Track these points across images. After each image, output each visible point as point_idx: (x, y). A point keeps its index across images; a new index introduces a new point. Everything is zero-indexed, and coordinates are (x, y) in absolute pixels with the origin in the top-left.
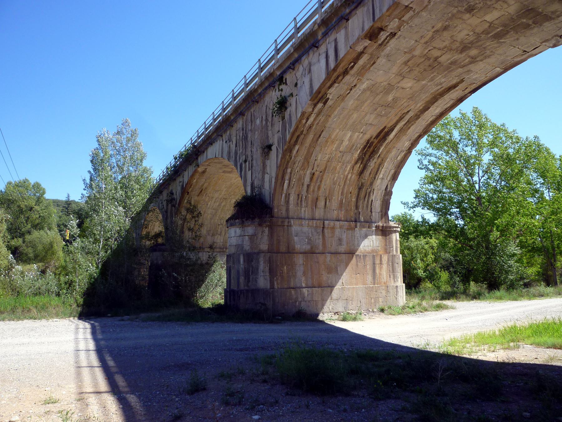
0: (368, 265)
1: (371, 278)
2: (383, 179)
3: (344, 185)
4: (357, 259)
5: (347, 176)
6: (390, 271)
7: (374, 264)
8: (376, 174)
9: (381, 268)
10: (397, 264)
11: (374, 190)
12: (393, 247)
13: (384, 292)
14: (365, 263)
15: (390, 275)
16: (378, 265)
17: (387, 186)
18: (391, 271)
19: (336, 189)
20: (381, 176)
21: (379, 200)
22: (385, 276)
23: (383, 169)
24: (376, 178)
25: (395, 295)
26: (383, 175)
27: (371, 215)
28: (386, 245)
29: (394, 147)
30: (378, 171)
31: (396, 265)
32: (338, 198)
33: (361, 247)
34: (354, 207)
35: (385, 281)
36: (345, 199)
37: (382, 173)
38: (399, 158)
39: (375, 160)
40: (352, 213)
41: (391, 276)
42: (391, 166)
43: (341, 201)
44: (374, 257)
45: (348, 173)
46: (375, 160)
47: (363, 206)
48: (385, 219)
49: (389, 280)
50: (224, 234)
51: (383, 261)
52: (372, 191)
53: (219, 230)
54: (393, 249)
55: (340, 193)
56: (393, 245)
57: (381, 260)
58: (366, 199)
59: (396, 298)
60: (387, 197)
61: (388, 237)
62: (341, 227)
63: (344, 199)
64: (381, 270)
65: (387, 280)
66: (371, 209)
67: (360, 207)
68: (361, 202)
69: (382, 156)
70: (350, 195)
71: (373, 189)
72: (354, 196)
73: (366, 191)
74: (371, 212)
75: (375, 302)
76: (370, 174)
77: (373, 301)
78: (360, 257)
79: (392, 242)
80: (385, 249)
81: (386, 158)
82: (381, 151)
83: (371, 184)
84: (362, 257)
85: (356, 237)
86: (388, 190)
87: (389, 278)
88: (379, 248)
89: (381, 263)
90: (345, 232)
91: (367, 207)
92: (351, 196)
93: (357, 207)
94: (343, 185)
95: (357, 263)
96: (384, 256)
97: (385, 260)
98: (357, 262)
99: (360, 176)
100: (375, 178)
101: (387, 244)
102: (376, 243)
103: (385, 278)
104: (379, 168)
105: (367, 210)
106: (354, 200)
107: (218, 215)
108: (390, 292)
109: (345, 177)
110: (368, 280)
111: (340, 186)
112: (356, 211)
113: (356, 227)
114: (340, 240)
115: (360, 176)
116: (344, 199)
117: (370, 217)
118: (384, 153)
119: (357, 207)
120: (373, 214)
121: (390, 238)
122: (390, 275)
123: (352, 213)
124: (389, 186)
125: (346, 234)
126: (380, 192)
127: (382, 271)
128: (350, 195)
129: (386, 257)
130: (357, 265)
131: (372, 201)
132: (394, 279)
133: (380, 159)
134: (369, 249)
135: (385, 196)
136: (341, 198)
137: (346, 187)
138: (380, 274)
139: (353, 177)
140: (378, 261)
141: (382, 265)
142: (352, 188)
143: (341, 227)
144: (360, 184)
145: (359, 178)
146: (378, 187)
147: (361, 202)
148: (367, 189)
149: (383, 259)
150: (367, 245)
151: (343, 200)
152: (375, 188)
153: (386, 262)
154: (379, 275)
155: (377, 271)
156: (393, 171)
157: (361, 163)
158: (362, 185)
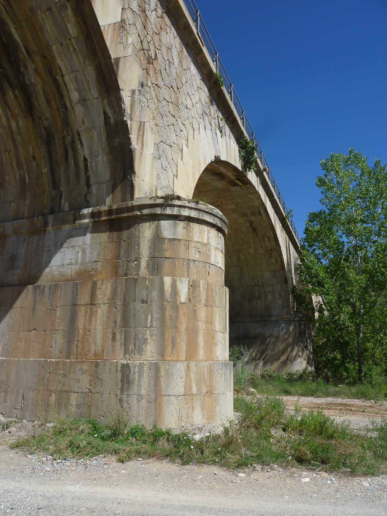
0: (58, 309)
1: (62, 341)
2: (83, 101)
3: (15, 146)
4: (35, 297)
5: (10, 127)
6: (115, 323)
7: (74, 305)
8: (61, 96)
9: (91, 316)
10: (143, 302)
11: (79, 135)
12: (138, 259)
13: (85, 380)
14: (53, 304)
15: (114, 334)
16: (83, 308)
17: (105, 113)
18: (118, 324)
19: (4, 160)
20: (75, 96)
21: (100, 152)
22: (99, 335)
23: (66, 78)
24: (69, 106)
25: (119, 392)
26: (78, 90)
27: (89, 191)
28: (118, 257)
29: (32, 10)
30: (58, 87)
31: (138, 305)
32: (15, 176)
33: (56, 260)
34: (49, 186)
35: (99, 348)
36: (28, 174)
37: (71, 86)
38: (72, 30)
39: (29, 67)
40: (46, 199)
41: (118, 337)
42: (76, 62)
43: (23, 179)
44: (77, 289)
45: (8, 120)
46: (30, 66)
47: (69, 178)
48: (124, 194)
49: (110, 349)
50: (264, 297)
51: (99, 297)
52: (76, 137)
53: (256, 293)
54: (138, 266)
55: (14, 164)
56: (139, 253)
57: (93, 295)
58: (71, 161)
59: (121, 400)
60: (117, 141)
61: (125, 233)
62: (16, 232)
63: (26, 175)
64: (90, 320)
65: (103, 346)
66: (88, 178)
67: (63, 181)
68: (62, 170)
69: (33, 47)
70: (34, 164)
71: (75, 132)
72: (43, 162)
73: (64, 142)
74: (88, 185)
75: (59, 403)
76: (48, 102)
77: (53, 399)
78: (44, 290)
79: (139, 245)
80: (115, 267)
81: (48, 47)
82: (16, 36)
83: (66, 122)
84: (47, 290)
85: (46, 248)
86: (112, 120)
87: (110, 341)
88: (99, 265)
89: (92, 304)
90: (24, 241)
91: (78, 176)
92: (37, 165)
93: (55, 184)
94: (12, 148)
95: (34, 305)
96: (102, 284)
97: (105, 295)
98: (35, 301)
99: (32, 115)
100: (66, 107)
101: (122, 253)
102: (92, 253)
103: (99, 341)
104: (55, 81)
105: (79, 183)
106: (45, 170)
107: (246, 274)
108: (102, 381)
109: (8, 130)
110: (54, 345)
111: (9, 152)
112: (54, 193)
113: (46, 224)
114: (13, 258)
115: (32, 115)
116: (26, 175)
117: (86, 196)
118: (29, 37)
119: (55, 184)
120: (94, 189)
121: (130, 238)
122: (114, 334)
123: (46, 199)
124: (110, 113)
125: (25, 244)
126: (95, 134)
127: (94, 323)
128: (34, 164)
129: (109, 287)
130: (34, 309)
131: (85, 160)
132: (126, 344)
133: (37, 58)
134: (70, 271)
135: (109, 138)
136: (20, 175)
137: (20, 149)
138: (87, 330)
139: (21, 123)
140: (84, 298)
141: (93, 307)
142: (33, 148)
143: (16, 232)
144: (44, 133)
145: (34, 120)
146: (83, 123)
147: (62, 170)
148: (64, 137)
149: (98, 292)
150: (68, 261)
151: (24, 178)
152: (80, 129)
153: (106, 298)
154: (85, 334)
155: (81, 323)
156: (91, 71)
157: (12, 86)
158: (48, 130)
